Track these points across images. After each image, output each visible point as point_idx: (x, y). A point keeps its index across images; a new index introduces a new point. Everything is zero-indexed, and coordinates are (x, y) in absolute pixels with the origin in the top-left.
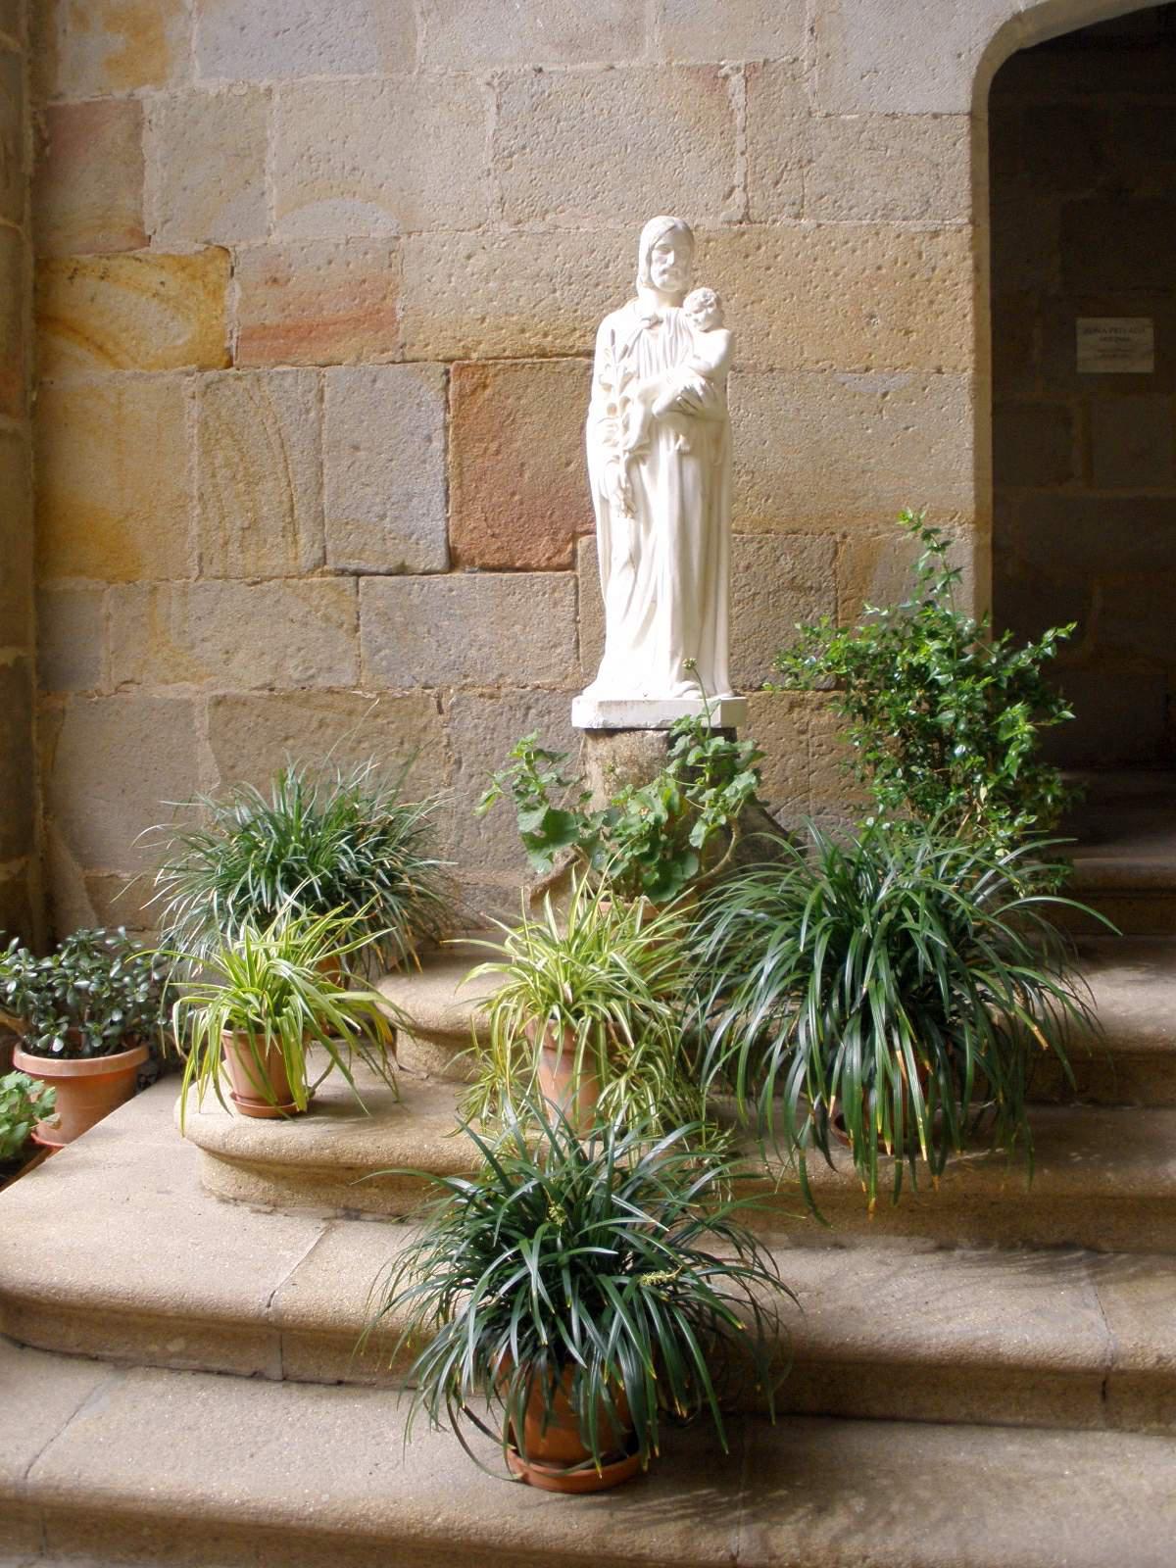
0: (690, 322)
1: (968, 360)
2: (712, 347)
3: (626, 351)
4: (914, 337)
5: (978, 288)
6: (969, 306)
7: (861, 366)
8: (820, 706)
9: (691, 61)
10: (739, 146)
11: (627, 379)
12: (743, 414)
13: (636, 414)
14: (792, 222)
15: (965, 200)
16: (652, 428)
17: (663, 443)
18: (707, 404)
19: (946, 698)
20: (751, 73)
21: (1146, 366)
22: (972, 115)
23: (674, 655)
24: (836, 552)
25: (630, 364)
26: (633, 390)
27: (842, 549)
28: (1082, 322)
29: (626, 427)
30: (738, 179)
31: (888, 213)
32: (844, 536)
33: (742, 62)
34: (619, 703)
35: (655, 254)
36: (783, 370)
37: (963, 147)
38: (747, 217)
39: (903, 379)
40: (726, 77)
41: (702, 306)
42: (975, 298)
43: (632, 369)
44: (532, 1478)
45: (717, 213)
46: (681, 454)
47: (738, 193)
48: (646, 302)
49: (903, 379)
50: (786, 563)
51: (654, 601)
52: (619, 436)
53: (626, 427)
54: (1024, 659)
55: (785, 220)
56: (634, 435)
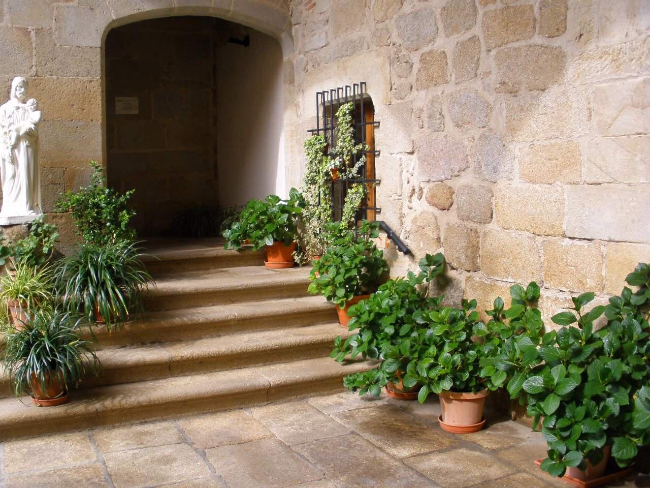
0: (29, 109)
1: (100, 117)
2: (36, 116)
3: (10, 116)
4: (85, 111)
5: (102, 97)
6: (100, 103)
7: (70, 119)
8: (61, 217)
9: (20, 26)
10: (34, 52)
11: (10, 124)
12: (42, 138)
13: (14, 135)
14: (49, 76)
15: (99, 72)
16: (19, 139)
17: (22, 143)
18: (35, 132)
19: (104, 211)
20: (38, 31)
21: (136, 112)
22: (101, 48)
23: (27, 203)
24: (64, 173)
25: (11, 120)
26: (13, 128)
27: (66, 172)
28: (117, 98)
29: (10, 139)
30: (34, 63)
31: (78, 75)
32: (66, 168)
33: (35, 28)
34: (14, 217)
35: (18, 88)
36: (48, 121)
37: (98, 57)
38: (37, 75)
39: (81, 123)
40: (30, 32)
41: (33, 104)
42: (102, 100)
43: (11, 122)
44: (43, 404)
45: (27, 73)
46: (27, 146)
47: (34, 68)
48: (13, 102)
49: (81, 123)
50: (50, 176)
51: (20, 188)
52: (8, 140)
53: (10, 139)
54: (122, 199)
55: (48, 76)
56: (13, 141)
